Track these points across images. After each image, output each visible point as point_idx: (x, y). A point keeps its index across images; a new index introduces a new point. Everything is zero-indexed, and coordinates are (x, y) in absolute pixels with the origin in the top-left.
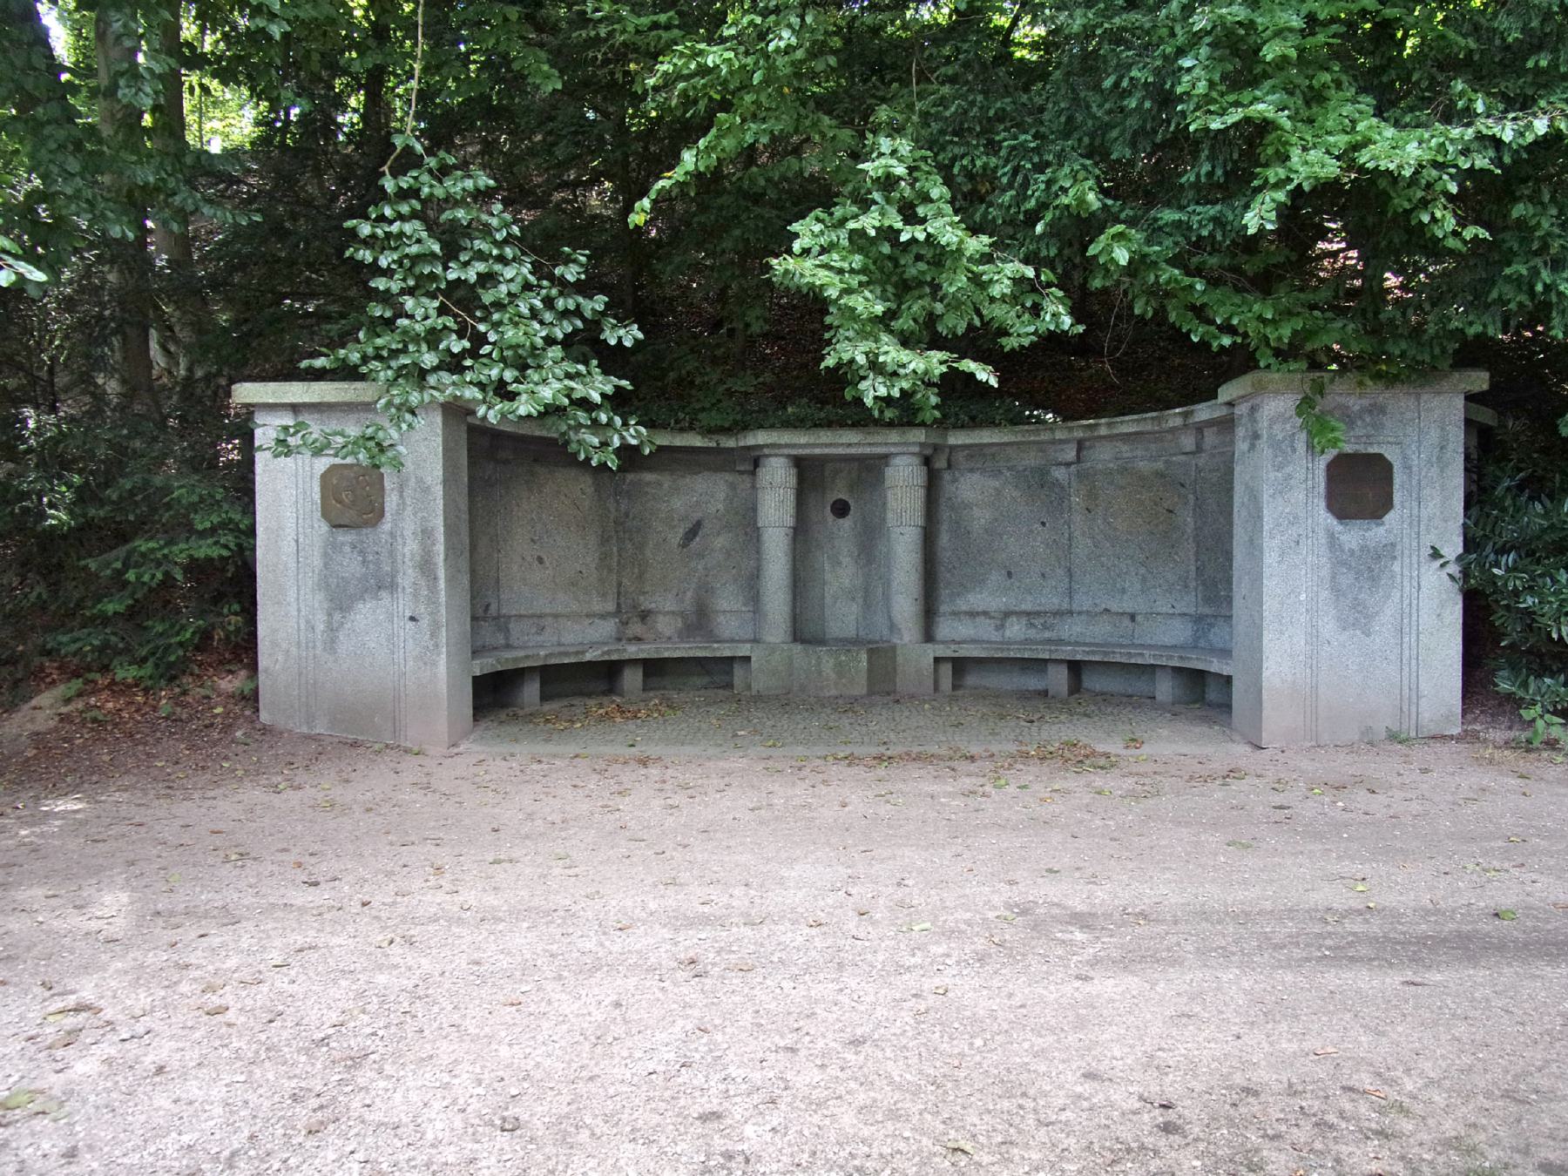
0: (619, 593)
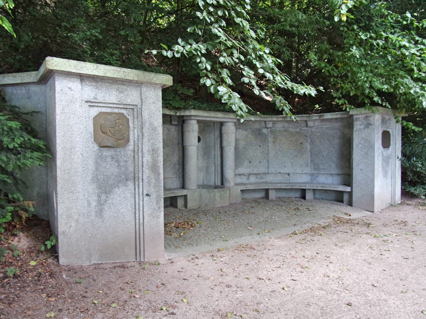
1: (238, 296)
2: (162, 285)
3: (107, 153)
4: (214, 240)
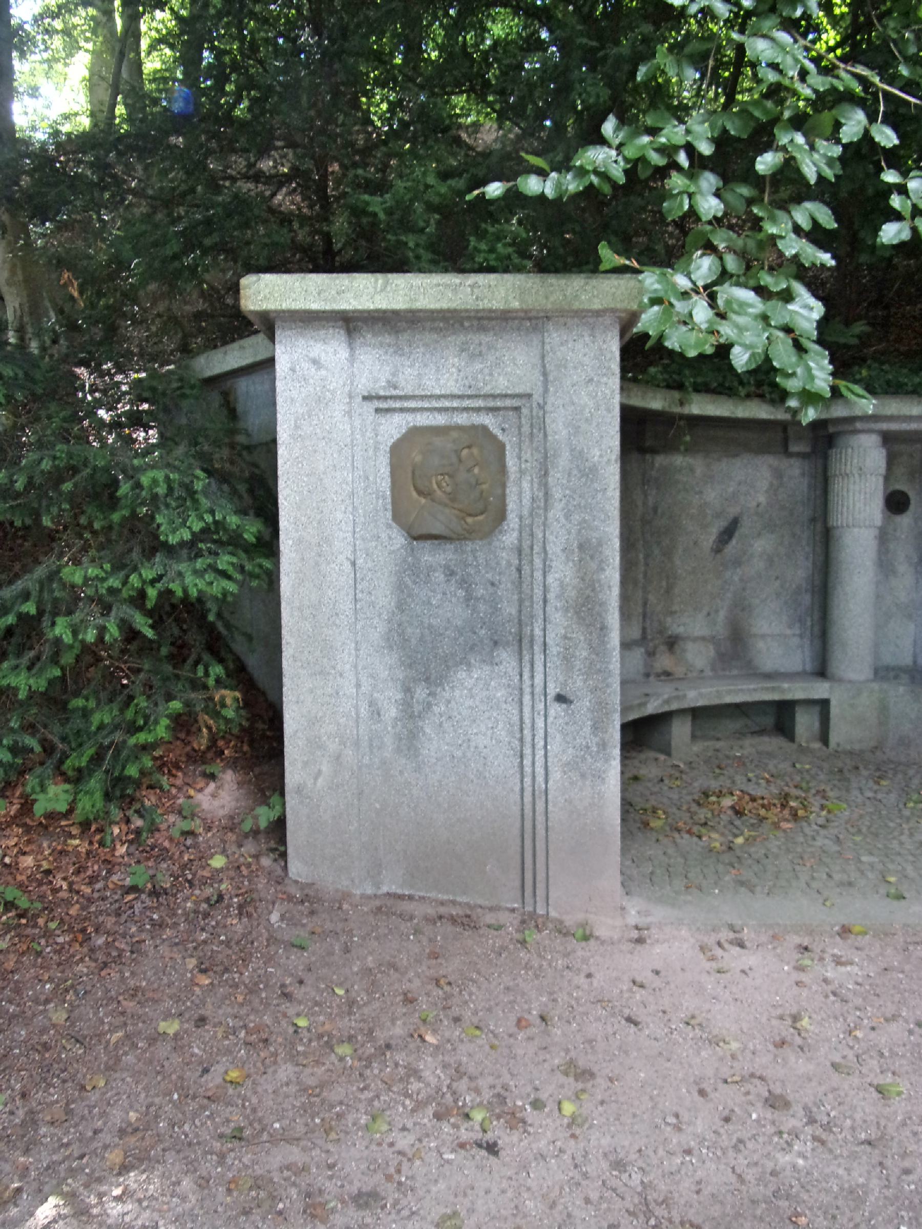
0: (644, 616)
1: (784, 1159)
2: (538, 1021)
3: (433, 557)
4: (850, 884)
